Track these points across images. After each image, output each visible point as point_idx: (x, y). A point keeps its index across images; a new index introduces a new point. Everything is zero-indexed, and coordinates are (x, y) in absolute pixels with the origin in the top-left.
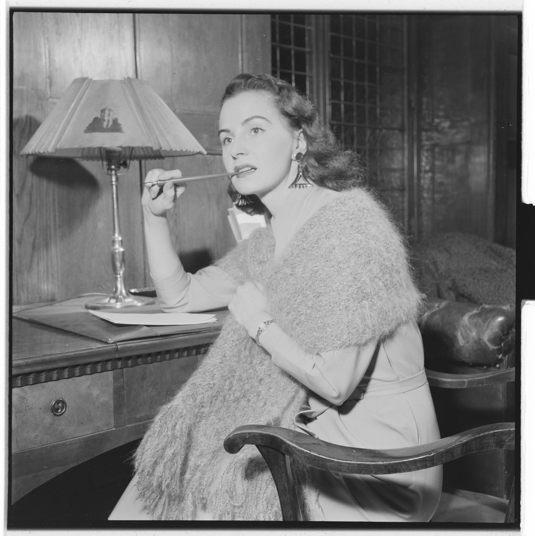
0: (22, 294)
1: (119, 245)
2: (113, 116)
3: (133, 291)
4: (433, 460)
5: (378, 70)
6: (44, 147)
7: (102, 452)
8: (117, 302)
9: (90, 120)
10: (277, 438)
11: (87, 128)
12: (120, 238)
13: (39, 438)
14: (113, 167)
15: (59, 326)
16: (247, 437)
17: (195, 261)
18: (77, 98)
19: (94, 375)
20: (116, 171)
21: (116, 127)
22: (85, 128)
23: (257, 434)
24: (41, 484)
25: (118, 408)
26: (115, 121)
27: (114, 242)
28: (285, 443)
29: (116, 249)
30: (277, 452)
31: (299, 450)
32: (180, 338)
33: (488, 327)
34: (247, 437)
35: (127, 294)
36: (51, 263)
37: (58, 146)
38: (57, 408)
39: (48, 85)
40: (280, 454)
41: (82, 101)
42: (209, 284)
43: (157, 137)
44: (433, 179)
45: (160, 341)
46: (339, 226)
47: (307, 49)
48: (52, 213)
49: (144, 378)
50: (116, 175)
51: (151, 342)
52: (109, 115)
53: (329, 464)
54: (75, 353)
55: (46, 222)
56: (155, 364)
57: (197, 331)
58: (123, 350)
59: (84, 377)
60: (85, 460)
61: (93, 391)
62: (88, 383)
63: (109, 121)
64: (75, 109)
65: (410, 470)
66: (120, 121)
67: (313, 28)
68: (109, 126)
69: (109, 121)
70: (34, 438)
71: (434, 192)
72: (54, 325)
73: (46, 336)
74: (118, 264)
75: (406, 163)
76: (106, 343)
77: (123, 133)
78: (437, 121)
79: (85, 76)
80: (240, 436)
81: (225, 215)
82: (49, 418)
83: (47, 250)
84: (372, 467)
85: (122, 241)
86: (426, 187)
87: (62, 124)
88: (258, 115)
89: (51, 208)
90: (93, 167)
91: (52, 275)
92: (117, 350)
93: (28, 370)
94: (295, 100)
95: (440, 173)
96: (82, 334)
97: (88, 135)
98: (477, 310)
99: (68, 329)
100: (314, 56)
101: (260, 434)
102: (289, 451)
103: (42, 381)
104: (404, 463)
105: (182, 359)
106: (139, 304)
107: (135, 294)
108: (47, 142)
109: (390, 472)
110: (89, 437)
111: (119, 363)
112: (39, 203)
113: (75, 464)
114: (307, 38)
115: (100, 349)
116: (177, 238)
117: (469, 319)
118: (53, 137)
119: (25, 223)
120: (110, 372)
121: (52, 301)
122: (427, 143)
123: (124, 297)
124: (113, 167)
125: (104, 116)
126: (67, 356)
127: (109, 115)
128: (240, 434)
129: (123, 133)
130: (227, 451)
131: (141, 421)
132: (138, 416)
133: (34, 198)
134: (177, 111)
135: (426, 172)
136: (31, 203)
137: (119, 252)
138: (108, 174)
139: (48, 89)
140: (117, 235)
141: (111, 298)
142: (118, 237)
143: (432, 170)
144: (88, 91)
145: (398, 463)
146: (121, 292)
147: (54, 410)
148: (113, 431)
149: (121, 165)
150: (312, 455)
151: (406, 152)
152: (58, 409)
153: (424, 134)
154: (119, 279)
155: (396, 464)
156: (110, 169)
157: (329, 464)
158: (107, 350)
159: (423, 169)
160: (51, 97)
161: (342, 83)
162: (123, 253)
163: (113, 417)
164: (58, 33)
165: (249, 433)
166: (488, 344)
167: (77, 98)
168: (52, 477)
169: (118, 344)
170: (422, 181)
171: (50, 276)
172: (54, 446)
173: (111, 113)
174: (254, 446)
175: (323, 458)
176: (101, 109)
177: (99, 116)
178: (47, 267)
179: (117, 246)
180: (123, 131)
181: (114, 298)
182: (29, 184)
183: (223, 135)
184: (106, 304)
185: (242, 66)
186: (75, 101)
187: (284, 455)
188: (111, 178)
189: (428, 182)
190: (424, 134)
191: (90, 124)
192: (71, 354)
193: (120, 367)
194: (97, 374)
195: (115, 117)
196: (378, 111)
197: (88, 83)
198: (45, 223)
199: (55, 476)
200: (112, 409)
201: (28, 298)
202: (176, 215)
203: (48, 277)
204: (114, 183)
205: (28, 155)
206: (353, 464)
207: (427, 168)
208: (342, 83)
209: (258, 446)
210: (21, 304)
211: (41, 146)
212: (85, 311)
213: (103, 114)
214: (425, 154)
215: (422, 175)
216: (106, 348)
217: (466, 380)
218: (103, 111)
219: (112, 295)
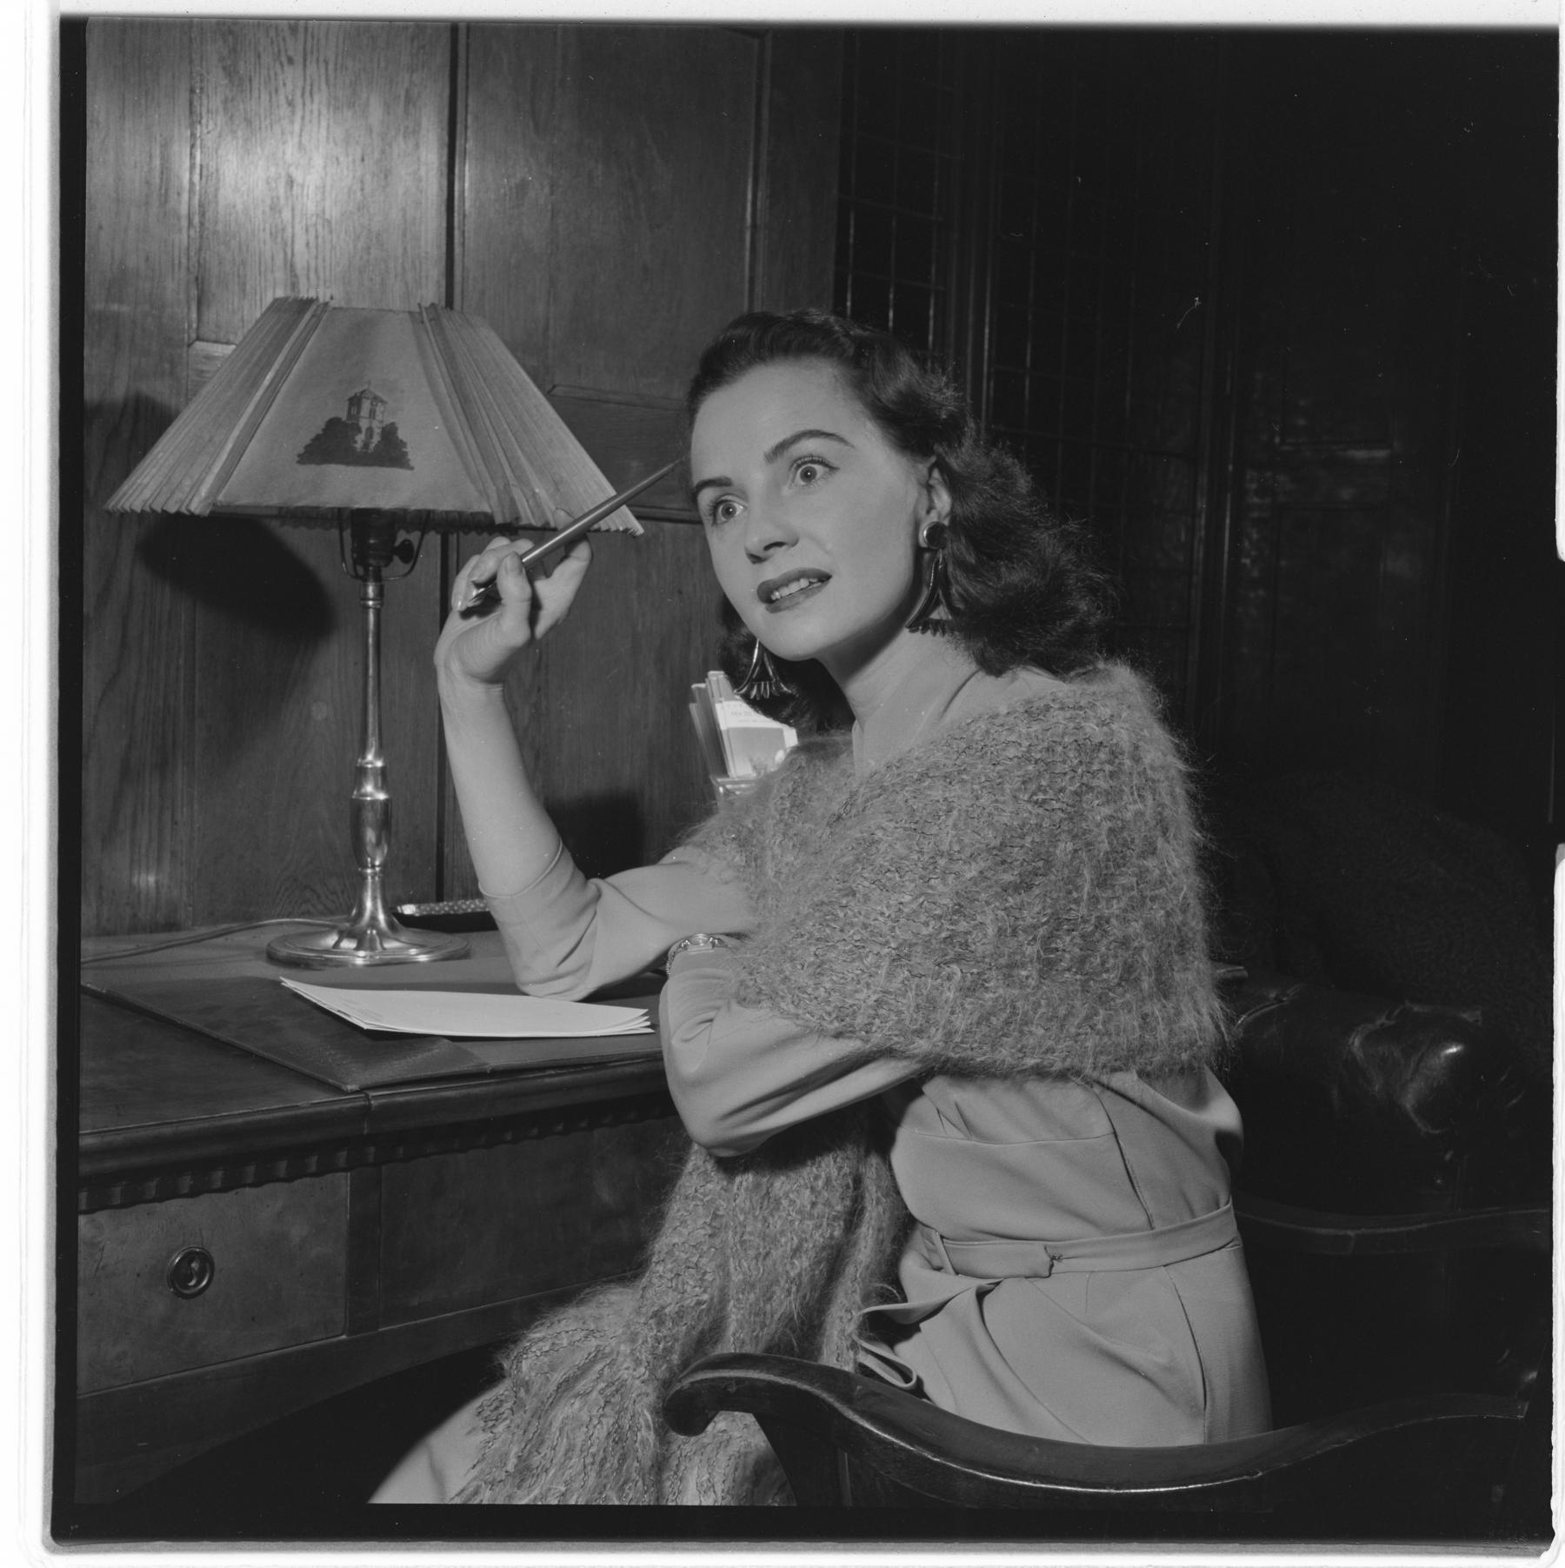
1: (376, 787)
2: (383, 417)
3: (409, 909)
6: (179, 495)
8: (358, 948)
9: (318, 426)
11: (307, 447)
16: (733, 1389)
17: (605, 834)
18: (280, 359)
19: (297, 1182)
21: (390, 452)
22: (301, 450)
26: (389, 433)
33: (1416, 1070)
35: (391, 925)
37: (220, 498)
38: (185, 1274)
42: (643, 911)
43: (507, 485)
45: (492, 1088)
51: (464, 1091)
58: (388, 1111)
59: (267, 1188)
61: (288, 1225)
63: (370, 431)
64: (273, 389)
66: (402, 434)
68: (372, 446)
74: (370, 835)
75: (1200, 553)
76: (337, 1090)
77: (412, 468)
79: (305, 293)
81: (679, 696)
88: (802, 428)
90: (319, 553)
91: (173, 854)
92: (366, 1111)
93: (111, 1164)
94: (905, 375)
97: (309, 471)
98: (1388, 1018)
99: (223, 1035)
101: (769, 1383)
106: (423, 958)
107: (408, 921)
108: (188, 483)
115: (319, 1109)
116: (537, 757)
117: (1362, 1045)
118: (209, 467)
123: (381, 935)
125: (358, 417)
127: (372, 414)
129: (412, 468)
134: (558, 391)
138: (357, 576)
140: (370, 757)
141: (344, 934)
142: (373, 760)
146: (374, 918)
147: (179, 1278)
148: (341, 1342)
160: (198, 339)
162: (386, 803)
164: (230, 72)
165: (739, 1380)
166: (1412, 1115)
167: (280, 359)
171: (167, 856)
173: (379, 408)
174: (750, 1418)
181: (350, 935)
183: (706, 497)
184: (327, 951)
185: (752, 268)
186: (276, 366)
188: (366, 587)
191: (318, 438)
193: (371, 1159)
194: (307, 1180)
201: (98, 916)
209: (763, 1421)
212: (266, 971)
216: (336, 1107)
217: (1351, 1233)
218: (355, 402)
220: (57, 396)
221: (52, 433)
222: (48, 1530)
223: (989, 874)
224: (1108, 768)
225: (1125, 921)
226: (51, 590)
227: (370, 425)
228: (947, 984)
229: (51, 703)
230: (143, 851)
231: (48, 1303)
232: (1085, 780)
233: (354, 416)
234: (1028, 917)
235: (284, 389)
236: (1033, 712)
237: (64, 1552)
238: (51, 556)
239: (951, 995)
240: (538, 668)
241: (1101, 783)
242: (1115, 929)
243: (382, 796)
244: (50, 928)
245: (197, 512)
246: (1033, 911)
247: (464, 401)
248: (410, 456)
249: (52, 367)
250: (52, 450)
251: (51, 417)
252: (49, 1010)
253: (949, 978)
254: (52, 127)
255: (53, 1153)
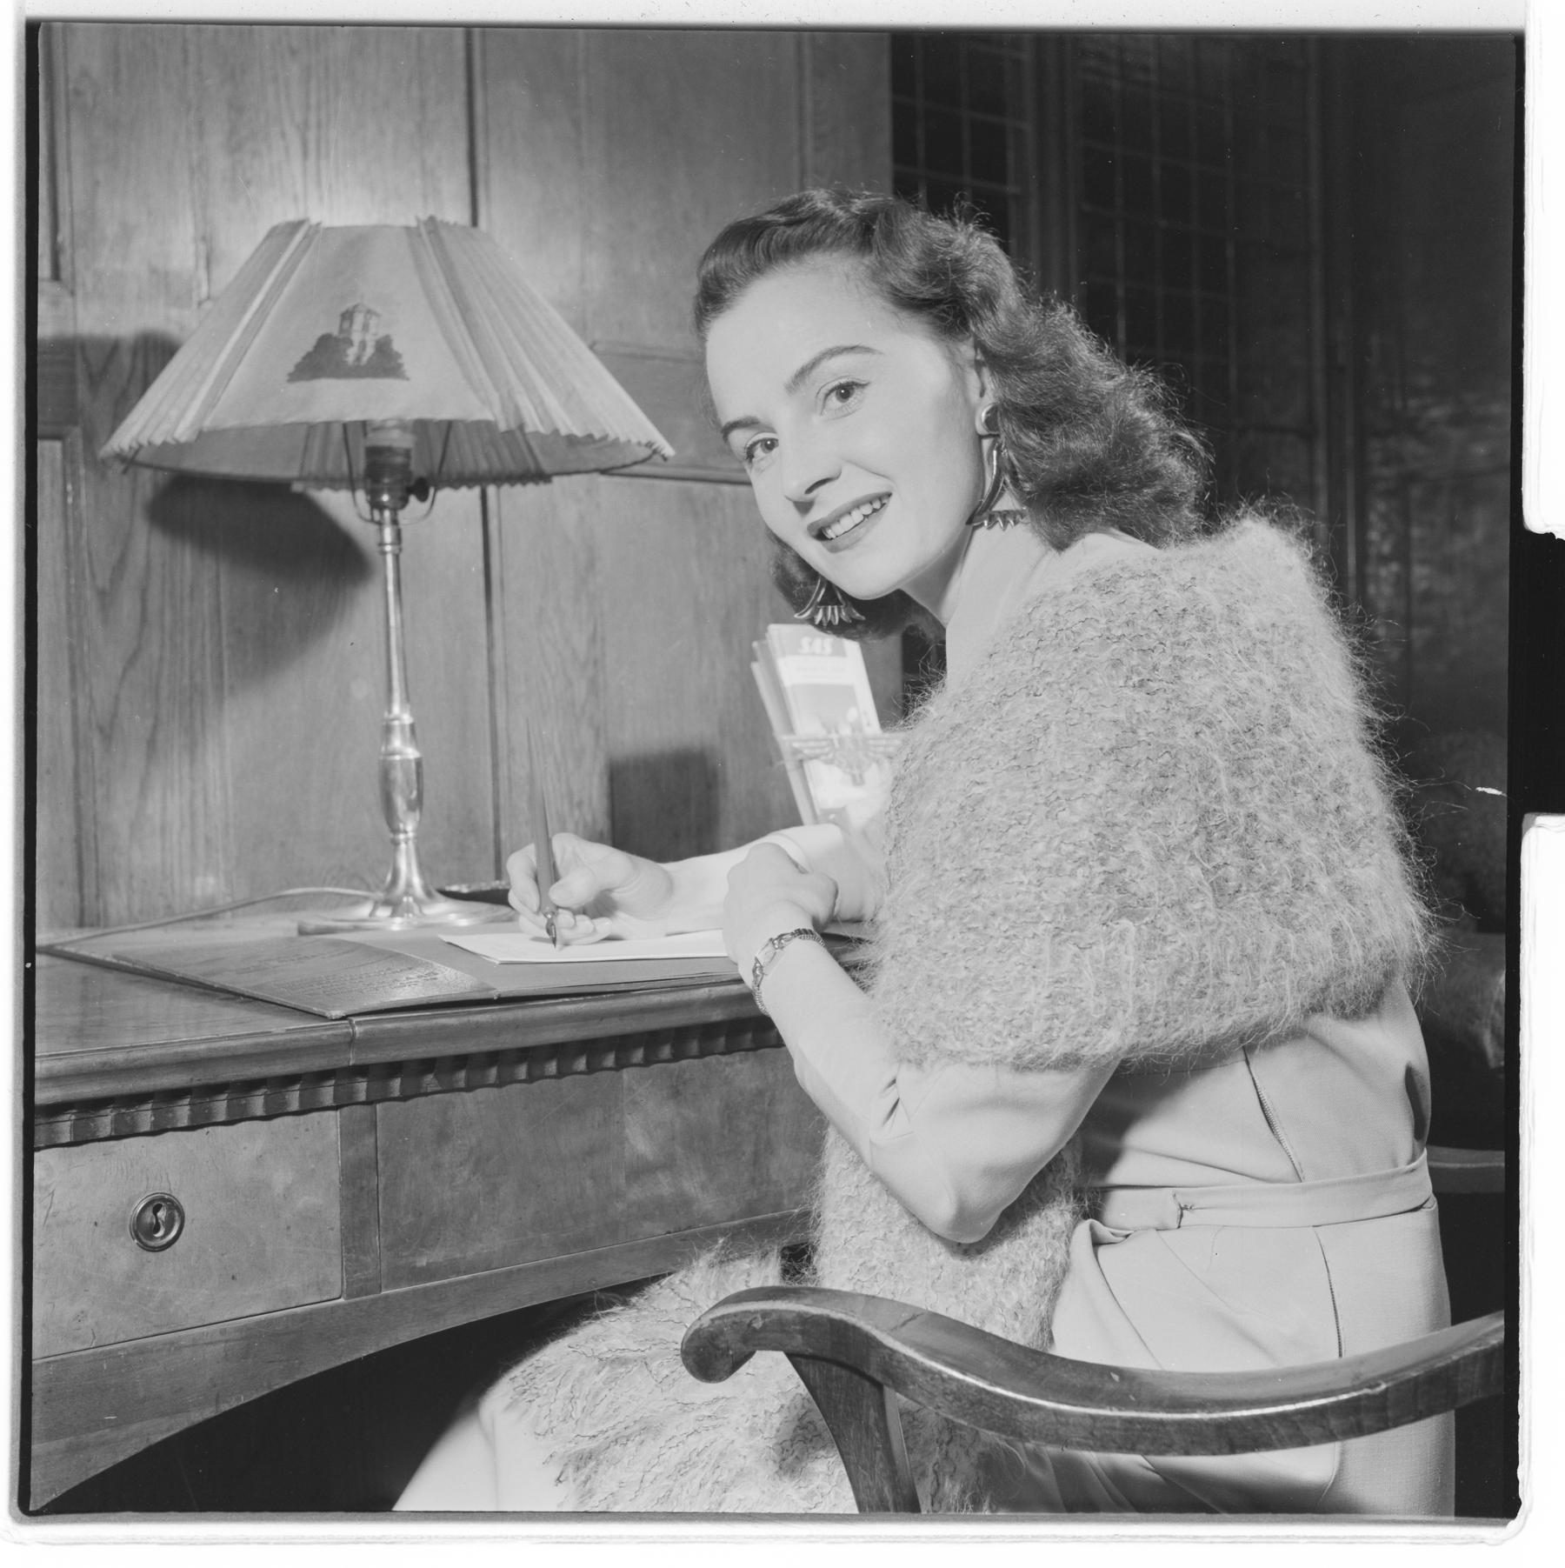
0: (112, 897)
1: (404, 741)
2: (377, 331)
4: (1384, 1409)
5: (1230, 251)
7: (299, 1377)
8: (393, 914)
9: (308, 345)
10: (855, 1329)
12: (407, 719)
13: (89, 1322)
14: (385, 498)
15: (193, 972)
16: (758, 1325)
20: (394, 511)
21: (385, 362)
22: (291, 368)
23: (790, 1317)
24: (92, 1473)
25: (354, 1235)
26: (384, 347)
27: (388, 730)
28: (880, 1345)
29: (393, 754)
30: (856, 1377)
31: (926, 1371)
32: (561, 1008)
34: (758, 1325)
35: (429, 894)
36: (206, 801)
37: (207, 424)
38: (156, 1223)
39: (202, 263)
40: (867, 1384)
41: (287, 290)
44: (1403, 583)
46: (1071, 655)
47: (1011, 189)
48: (208, 650)
49: (443, 1136)
50: (395, 522)
52: (365, 327)
53: (1028, 1417)
54: (214, 1045)
55: (191, 678)
56: (481, 1093)
57: (623, 988)
58: (369, 1042)
60: (243, 1401)
62: (259, 1146)
63: (363, 345)
64: (263, 311)
65: (1305, 1442)
66: (397, 346)
67: (1028, 127)
68: (365, 359)
69: (363, 345)
70: (66, 1322)
71: (1408, 621)
72: (180, 972)
73: (158, 1003)
74: (400, 803)
76: (322, 1017)
78: (1413, 403)
80: (736, 1322)
82: (125, 1254)
83: (192, 762)
84: (1172, 1429)
85: (412, 727)
86: (1382, 605)
87: (223, 357)
88: (830, 345)
89: (207, 633)
91: (208, 840)
92: (351, 1041)
95: (1423, 562)
96: (256, 993)
97: (302, 387)
100: (1033, 207)
102: (894, 1372)
103: (102, 1134)
104: (1283, 1416)
105: (567, 1081)
108: (174, 413)
109: (1233, 1449)
110: (259, 1323)
111: (361, 1087)
112: (168, 617)
113: (209, 1413)
114: (1011, 156)
116: (597, 735)
118: (193, 397)
119: (123, 677)
120: (332, 1113)
121: (209, 915)
122: (1386, 472)
124: (385, 498)
125: (349, 331)
126: (185, 1054)
127: (365, 327)
128: (735, 1315)
130: (692, 1373)
131: (432, 1277)
132: (422, 1262)
133: (154, 605)
135: (1384, 560)
136: (144, 619)
137: (402, 762)
138: (372, 520)
139: (202, 274)
140: (396, 709)
141: (376, 904)
142: (402, 715)
143: (1402, 554)
144: (304, 260)
145: (1264, 1416)
146: (409, 885)
148: (338, 1306)
149: (410, 491)
150: (969, 1386)
151: (1322, 500)
152: (157, 1229)
153: (1375, 444)
154: (403, 846)
155: (1255, 1419)
156: (376, 505)
157: (1028, 1417)
158: (319, 1039)
159: (1373, 551)
161: (1120, 292)
162: (419, 763)
163: (337, 1261)
165: (765, 1314)
168: (132, 1452)
169: (355, 1020)
170: (1372, 589)
172: (141, 1351)
173: (373, 322)
174: (781, 1355)
175: (1007, 1398)
176: (343, 309)
177: (335, 332)
178: (193, 815)
179: (397, 743)
180: (408, 374)
181: (386, 903)
182: (137, 559)
184: (364, 920)
187: (879, 1387)
188: (381, 531)
189: (1387, 590)
190: (1375, 444)
191: (309, 356)
192: (197, 1048)
193: (362, 1097)
195: (382, 333)
196: (1233, 373)
197: (305, 237)
198: (186, 681)
199: (142, 1447)
200: (335, 1236)
201: (129, 907)
202: (595, 663)
203: (193, 845)
204: (388, 548)
205: (130, 461)
206: (1107, 1418)
207: (1386, 548)
208: (1120, 292)
210: (106, 926)
211: (157, 427)
213: (346, 325)
214: (1381, 506)
215: (1370, 569)
218: (347, 316)
219: (380, 895)
220: (23, 185)
221: (18, 404)
222: (15, 1500)
223: (1115, 786)
224: (1199, 636)
225: (1275, 815)
226: (17, 561)
227: (362, 341)
228: (1122, 948)
229: (18, 175)
230: (175, 837)
231: (15, 1273)
232: (1176, 652)
233: (345, 332)
234: (1177, 834)
235: (273, 312)
236: (1105, 585)
237: (30, 1523)
238: (17, 527)
239: (1131, 958)
240: (593, 639)
241: (1196, 652)
242: (1267, 824)
243: (412, 753)
244: (16, 899)
245: (183, 439)
246: (1182, 822)
247: (465, 309)
248: (406, 367)
249: (18, 338)
250: (18, 421)
251: (17, 387)
252: (16, 981)
253: (1122, 937)
254: (18, 97)
255: (21, 1124)
